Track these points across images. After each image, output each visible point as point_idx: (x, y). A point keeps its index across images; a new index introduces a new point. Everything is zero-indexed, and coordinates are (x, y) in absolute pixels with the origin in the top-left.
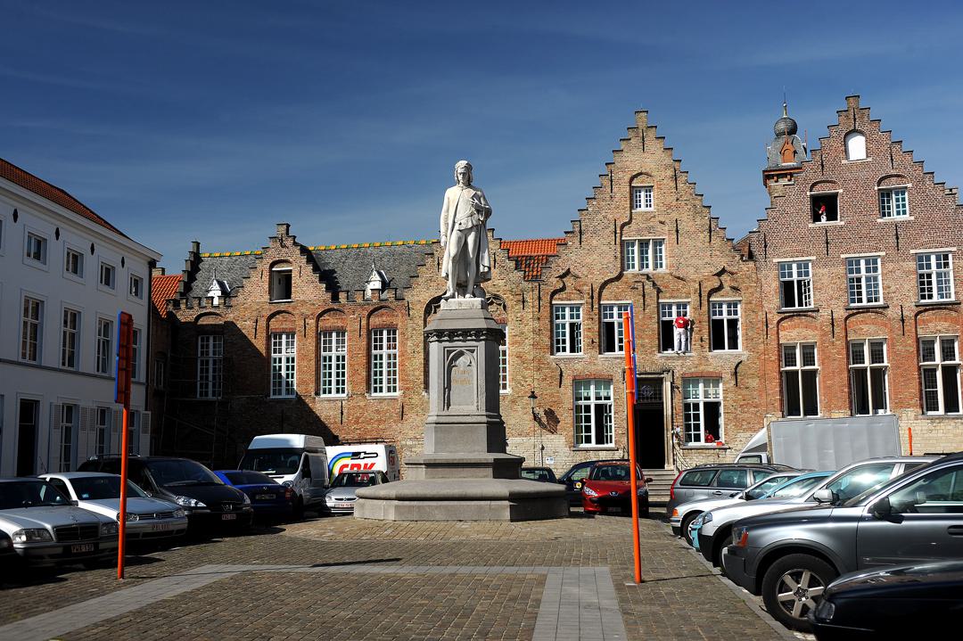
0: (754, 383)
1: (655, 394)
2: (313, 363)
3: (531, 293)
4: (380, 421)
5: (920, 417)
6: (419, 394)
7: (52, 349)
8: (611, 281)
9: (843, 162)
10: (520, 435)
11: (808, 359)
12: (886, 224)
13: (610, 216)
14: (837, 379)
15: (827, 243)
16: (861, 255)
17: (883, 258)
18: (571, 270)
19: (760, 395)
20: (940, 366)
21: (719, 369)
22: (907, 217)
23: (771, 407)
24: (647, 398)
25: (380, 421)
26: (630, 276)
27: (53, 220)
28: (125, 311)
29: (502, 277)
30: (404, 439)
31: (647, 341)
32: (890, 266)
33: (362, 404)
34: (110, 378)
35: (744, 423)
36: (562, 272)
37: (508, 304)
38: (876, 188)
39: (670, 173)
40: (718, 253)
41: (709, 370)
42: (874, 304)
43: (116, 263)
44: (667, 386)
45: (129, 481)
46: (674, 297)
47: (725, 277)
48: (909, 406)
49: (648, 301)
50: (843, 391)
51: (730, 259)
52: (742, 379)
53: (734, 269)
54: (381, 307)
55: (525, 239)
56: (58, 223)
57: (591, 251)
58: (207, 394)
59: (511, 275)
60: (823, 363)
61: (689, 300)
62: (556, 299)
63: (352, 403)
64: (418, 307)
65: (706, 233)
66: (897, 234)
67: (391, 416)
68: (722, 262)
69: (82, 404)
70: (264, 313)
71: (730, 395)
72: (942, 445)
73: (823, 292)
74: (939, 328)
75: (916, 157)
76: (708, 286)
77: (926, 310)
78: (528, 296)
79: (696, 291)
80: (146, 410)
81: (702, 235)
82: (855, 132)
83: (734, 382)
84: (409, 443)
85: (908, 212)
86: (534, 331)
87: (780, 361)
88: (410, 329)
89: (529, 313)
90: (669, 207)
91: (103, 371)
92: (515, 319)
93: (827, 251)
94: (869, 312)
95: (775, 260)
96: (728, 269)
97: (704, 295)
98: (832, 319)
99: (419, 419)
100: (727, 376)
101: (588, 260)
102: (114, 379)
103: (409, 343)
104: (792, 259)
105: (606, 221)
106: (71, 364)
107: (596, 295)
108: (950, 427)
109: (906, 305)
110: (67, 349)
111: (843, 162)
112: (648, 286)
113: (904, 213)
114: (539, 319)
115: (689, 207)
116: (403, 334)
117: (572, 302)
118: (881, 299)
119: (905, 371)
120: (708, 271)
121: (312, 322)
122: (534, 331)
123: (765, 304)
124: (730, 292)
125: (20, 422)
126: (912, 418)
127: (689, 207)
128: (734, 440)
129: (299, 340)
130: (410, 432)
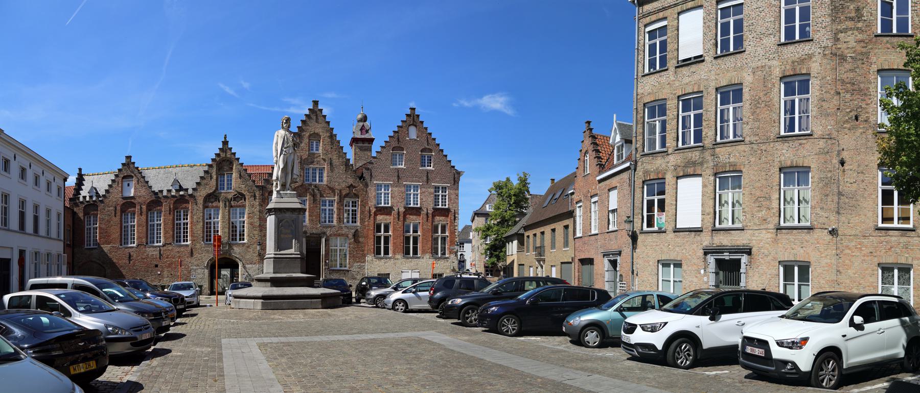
2: (145, 228)
9: (407, 139)
10: (251, 264)
11: (386, 230)
14: (399, 240)
25: (179, 257)
27: (13, 150)
32: (424, 190)
33: (170, 248)
34: (61, 240)
39: (328, 134)
40: (349, 176)
43: (27, 166)
45: (103, 290)
46: (328, 197)
58: (90, 245)
63: (165, 248)
67: (185, 255)
68: (350, 181)
76: (344, 193)
80: (64, 253)
83: (353, 239)
85: (432, 166)
87: (374, 230)
88: (195, 210)
96: (354, 184)
100: (350, 236)
103: (195, 217)
106: (5, 225)
111: (407, 139)
113: (430, 166)
118: (419, 204)
121: (144, 207)
126: (428, 258)
128: (352, 266)
129: (138, 216)
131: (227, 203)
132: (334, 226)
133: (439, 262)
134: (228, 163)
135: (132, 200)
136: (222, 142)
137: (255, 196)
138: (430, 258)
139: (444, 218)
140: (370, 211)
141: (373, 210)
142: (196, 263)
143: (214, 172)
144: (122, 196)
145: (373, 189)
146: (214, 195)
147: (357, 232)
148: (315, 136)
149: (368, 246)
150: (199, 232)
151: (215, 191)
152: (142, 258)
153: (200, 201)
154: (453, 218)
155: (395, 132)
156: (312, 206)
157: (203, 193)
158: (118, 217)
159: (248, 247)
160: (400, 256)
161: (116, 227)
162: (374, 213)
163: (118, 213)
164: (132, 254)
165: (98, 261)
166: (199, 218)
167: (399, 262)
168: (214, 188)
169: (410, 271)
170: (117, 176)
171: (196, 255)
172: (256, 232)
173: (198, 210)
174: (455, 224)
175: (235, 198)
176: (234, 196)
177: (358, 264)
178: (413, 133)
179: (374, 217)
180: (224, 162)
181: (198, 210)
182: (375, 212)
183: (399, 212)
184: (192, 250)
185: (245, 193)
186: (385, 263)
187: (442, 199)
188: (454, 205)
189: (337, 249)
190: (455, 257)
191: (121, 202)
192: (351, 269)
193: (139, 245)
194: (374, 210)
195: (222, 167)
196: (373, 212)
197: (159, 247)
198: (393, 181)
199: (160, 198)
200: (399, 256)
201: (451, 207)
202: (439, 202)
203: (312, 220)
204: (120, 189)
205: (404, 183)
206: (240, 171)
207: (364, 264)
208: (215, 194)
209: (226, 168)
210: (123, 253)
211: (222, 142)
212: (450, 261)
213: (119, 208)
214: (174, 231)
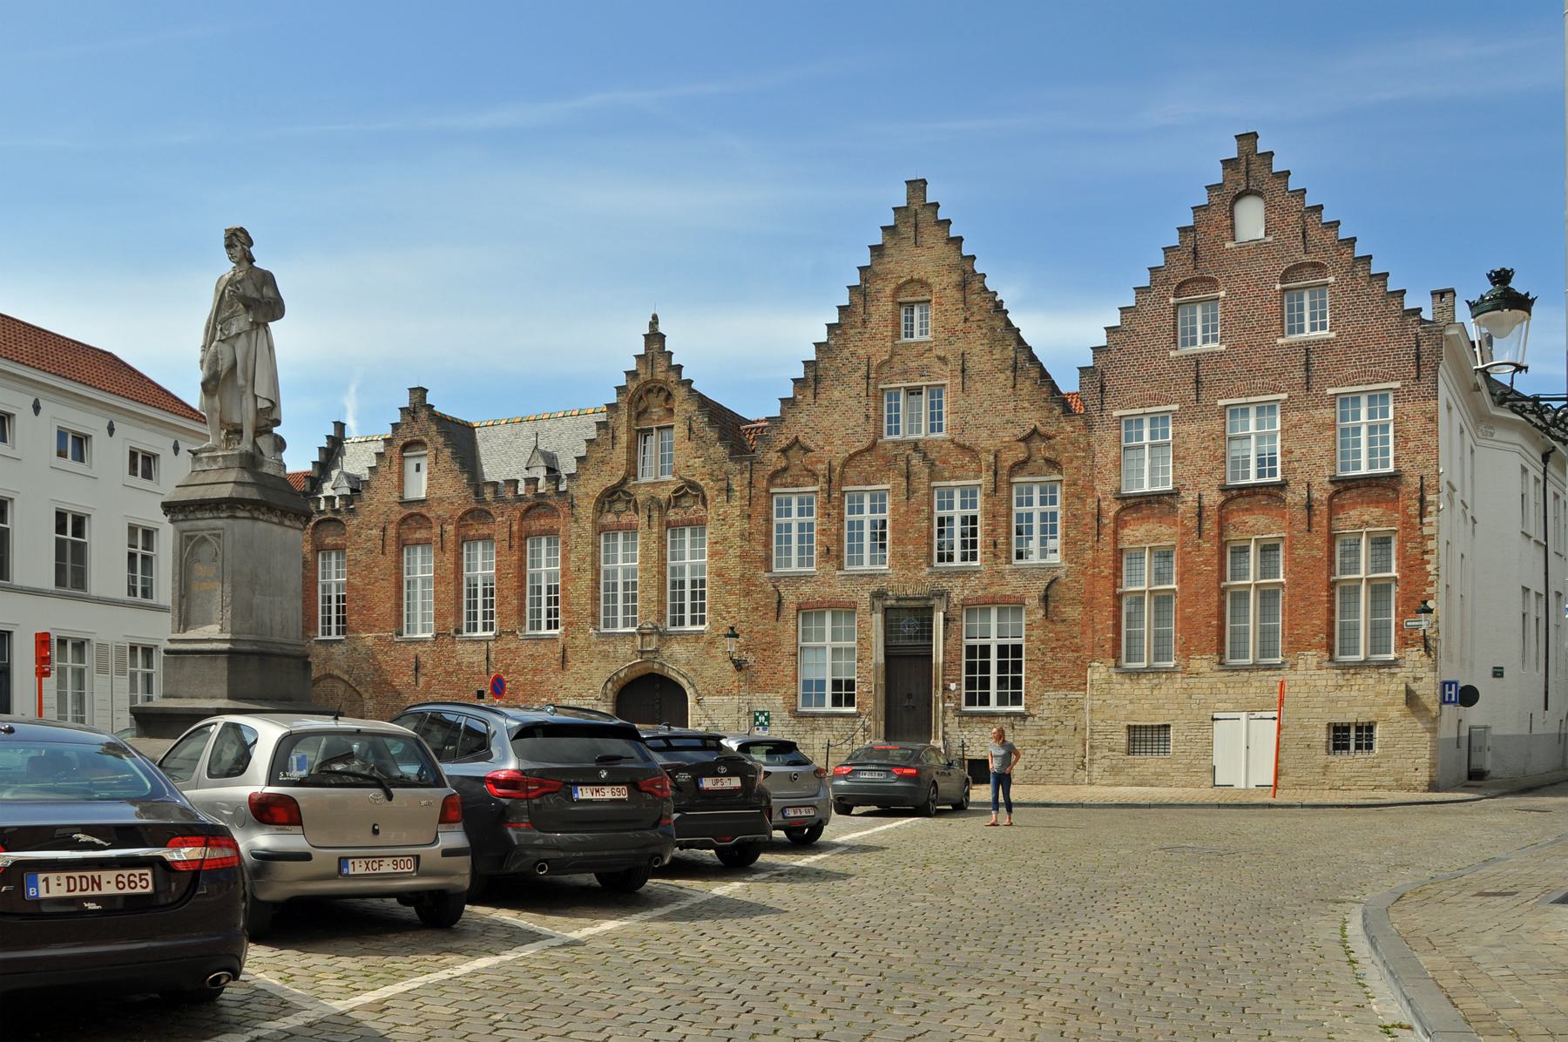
2: (452, 587)
4: (535, 671)
5: (1325, 664)
6: (585, 632)
8: (860, 453)
9: (1228, 245)
10: (719, 693)
12: (1290, 346)
13: (861, 352)
17: (1284, 402)
18: (800, 438)
19: (1083, 633)
20: (1364, 581)
21: (1021, 591)
22: (1325, 334)
23: (1098, 651)
25: (535, 671)
26: (889, 446)
30: (565, 696)
32: (1295, 417)
33: (513, 646)
35: (1056, 676)
36: (785, 443)
39: (955, 277)
40: (1026, 405)
41: (1004, 593)
42: (1267, 480)
44: (938, 618)
46: (957, 478)
47: (1037, 443)
48: (1310, 646)
50: (1209, 625)
51: (1046, 413)
52: (1055, 607)
53: (1050, 430)
54: (538, 505)
57: (833, 405)
60: (1181, 581)
61: (979, 481)
62: (776, 486)
63: (500, 645)
64: (585, 502)
67: (549, 665)
68: (1031, 419)
69: (95, 640)
70: (392, 517)
71: (1035, 632)
73: (1188, 462)
74: (1366, 518)
75: (1344, 233)
76: (1009, 459)
77: (1347, 489)
78: (736, 483)
79: (989, 467)
81: (1002, 376)
82: (1247, 193)
83: (1042, 612)
86: (742, 536)
90: (953, 332)
93: (1198, 394)
94: (1255, 494)
96: (1042, 429)
97: (1004, 472)
98: (1199, 507)
100: (1033, 602)
101: (826, 423)
102: (1531, 732)
103: (573, 557)
104: (1141, 411)
105: (855, 360)
108: (1371, 681)
109: (1316, 481)
110: (69, 564)
111: (1228, 245)
112: (916, 460)
113: (1323, 327)
114: (749, 516)
115: (984, 331)
116: (564, 543)
120: (1007, 435)
121: (450, 528)
122: (742, 536)
123: (1099, 487)
124: (1045, 468)
127: (984, 331)
128: (1039, 702)
131: (655, 514)
132: (975, 572)
133: (1359, 679)
134: (663, 395)
135: (424, 511)
136: (645, 335)
137: (729, 490)
138: (1320, 669)
139: (1377, 512)
140: (1099, 516)
141: (1111, 508)
142: (575, 689)
143: (622, 421)
144: (401, 497)
145: (1110, 436)
146: (624, 492)
147: (1055, 586)
148: (909, 296)
149: (1095, 631)
150: (583, 601)
151: (624, 481)
152: (446, 672)
153: (586, 509)
154: (1414, 509)
155: (1183, 230)
156: (902, 510)
157: (595, 485)
158: (391, 557)
159: (711, 643)
160: (1205, 663)
161: (385, 584)
162: (1117, 517)
163: (391, 548)
164: (423, 659)
165: (346, 677)
166: (584, 561)
167: (1204, 683)
168: (622, 473)
169: (1243, 716)
170: (388, 441)
171: (575, 665)
172: (731, 599)
173: (580, 536)
174: (1427, 531)
175: (679, 496)
176: (676, 492)
177: (1061, 694)
178: (1251, 220)
179: (1115, 533)
180: (651, 395)
181: (580, 536)
182: (1118, 513)
183: (1201, 508)
184: (564, 650)
185: (702, 483)
186: (1152, 689)
187: (1371, 442)
188: (1419, 458)
189: (988, 647)
190: (1425, 659)
191: (398, 513)
192: (1032, 711)
193: (438, 634)
194: (1116, 507)
195: (645, 411)
196: (1112, 514)
197: (487, 641)
198: (1182, 401)
199: (488, 504)
200: (1202, 663)
201: (1405, 467)
202: (1357, 454)
203: (904, 556)
204: (395, 479)
205: (1221, 403)
206: (690, 418)
207: (1079, 694)
208: (625, 489)
209: (657, 412)
210: (401, 657)
211: (645, 335)
212: (1401, 673)
213: (391, 532)
214: (522, 597)
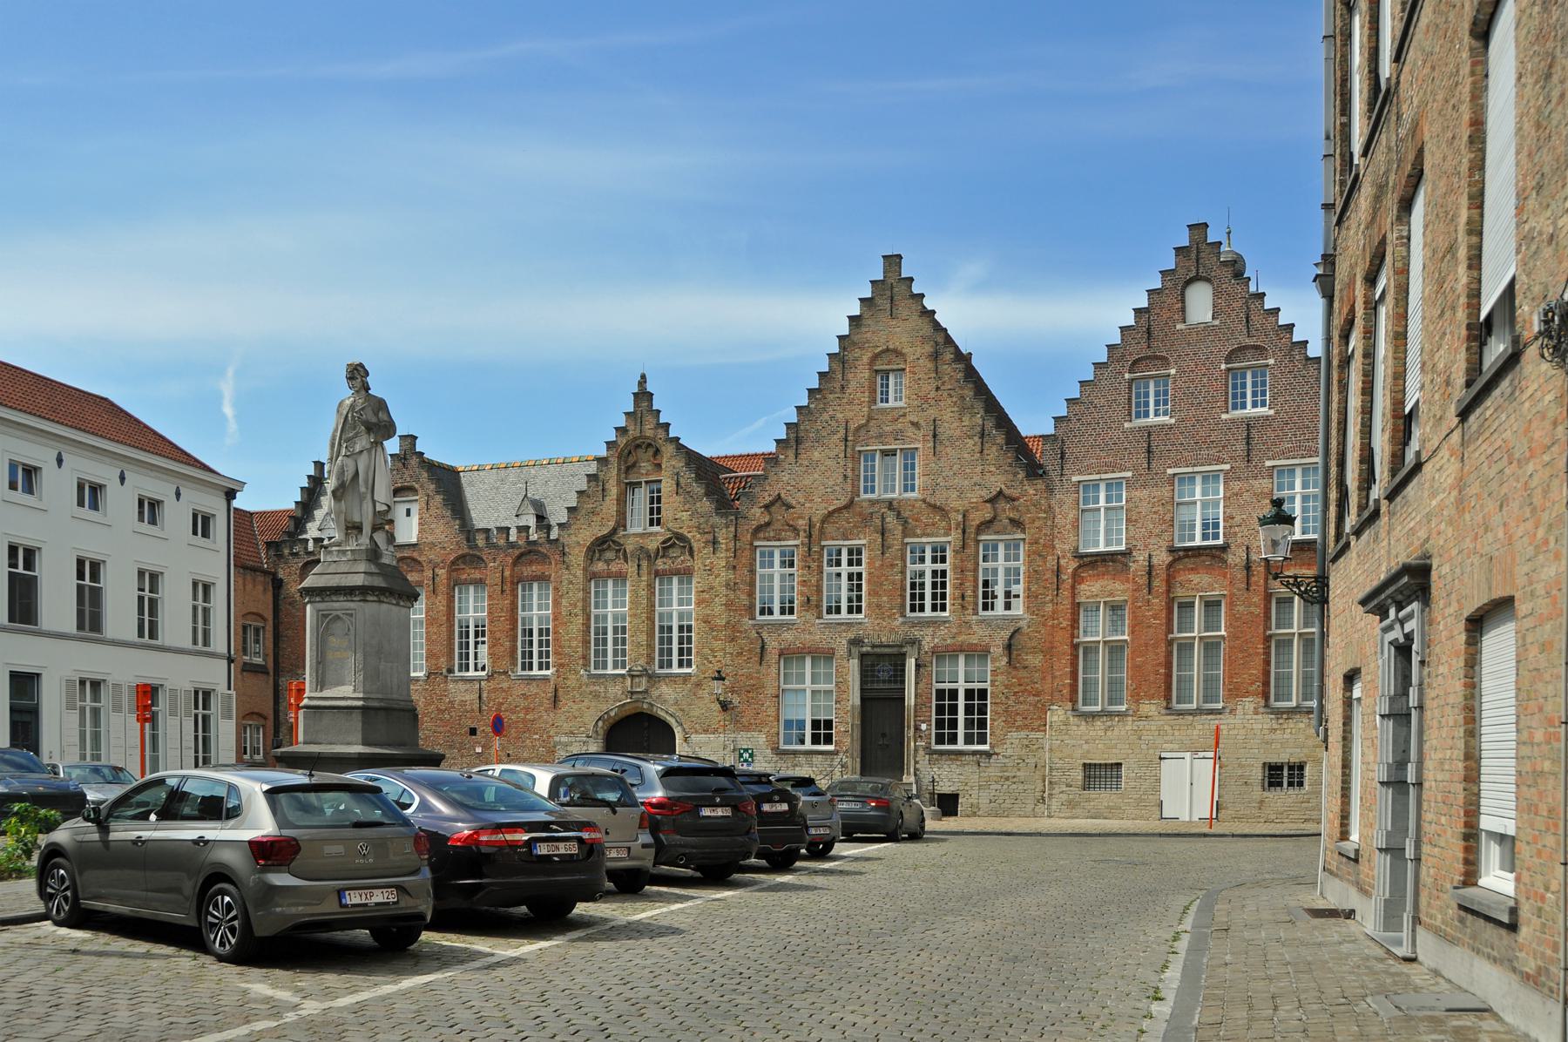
0: (1035, 660)
1: (895, 676)
3: (724, 530)
4: (527, 710)
5: (1261, 710)
7: (120, 615)
8: (839, 510)
9: (1179, 326)
10: (706, 731)
12: (1233, 421)
13: (839, 416)
15: (1149, 452)
16: (1197, 469)
19: (1044, 678)
21: (987, 640)
24: (884, 682)
25: (527, 710)
28: (1361, 595)
29: (686, 507)
31: (885, 598)
33: (505, 685)
34: (213, 655)
35: (1019, 718)
36: (768, 499)
37: (695, 546)
38: (1223, 367)
39: (928, 348)
40: (993, 469)
42: (1211, 542)
44: (911, 664)
46: (928, 535)
47: (1002, 504)
48: (1247, 694)
49: (890, 541)
53: (1014, 493)
54: (530, 552)
55: (1032, 435)
56: (61, 446)
57: (813, 465)
59: (698, 505)
61: (949, 539)
62: (759, 539)
63: (492, 684)
64: (576, 551)
65: (976, 439)
66: (1248, 437)
67: (541, 704)
68: (997, 482)
69: (111, 680)
71: (1000, 678)
72: (1287, 750)
73: (1139, 525)
76: (976, 518)
79: (958, 525)
81: (971, 442)
83: (1005, 659)
84: (564, 739)
86: (727, 585)
89: (720, 560)
90: (925, 399)
91: (151, 637)
92: (702, 568)
93: (1149, 463)
95: (1075, 479)
96: (1007, 492)
97: (971, 530)
98: (1149, 566)
99: (575, 707)
100: (997, 650)
101: (806, 482)
103: (564, 602)
104: (1097, 477)
106: (153, 635)
107: (815, 532)
108: (1302, 725)
111: (1179, 326)
112: (891, 519)
113: (1263, 404)
114: (734, 567)
115: (954, 399)
117: (783, 543)
119: (1246, 642)
120: (975, 496)
121: (442, 572)
122: (727, 585)
125: (11, 699)
128: (1002, 741)
130: (565, 725)
